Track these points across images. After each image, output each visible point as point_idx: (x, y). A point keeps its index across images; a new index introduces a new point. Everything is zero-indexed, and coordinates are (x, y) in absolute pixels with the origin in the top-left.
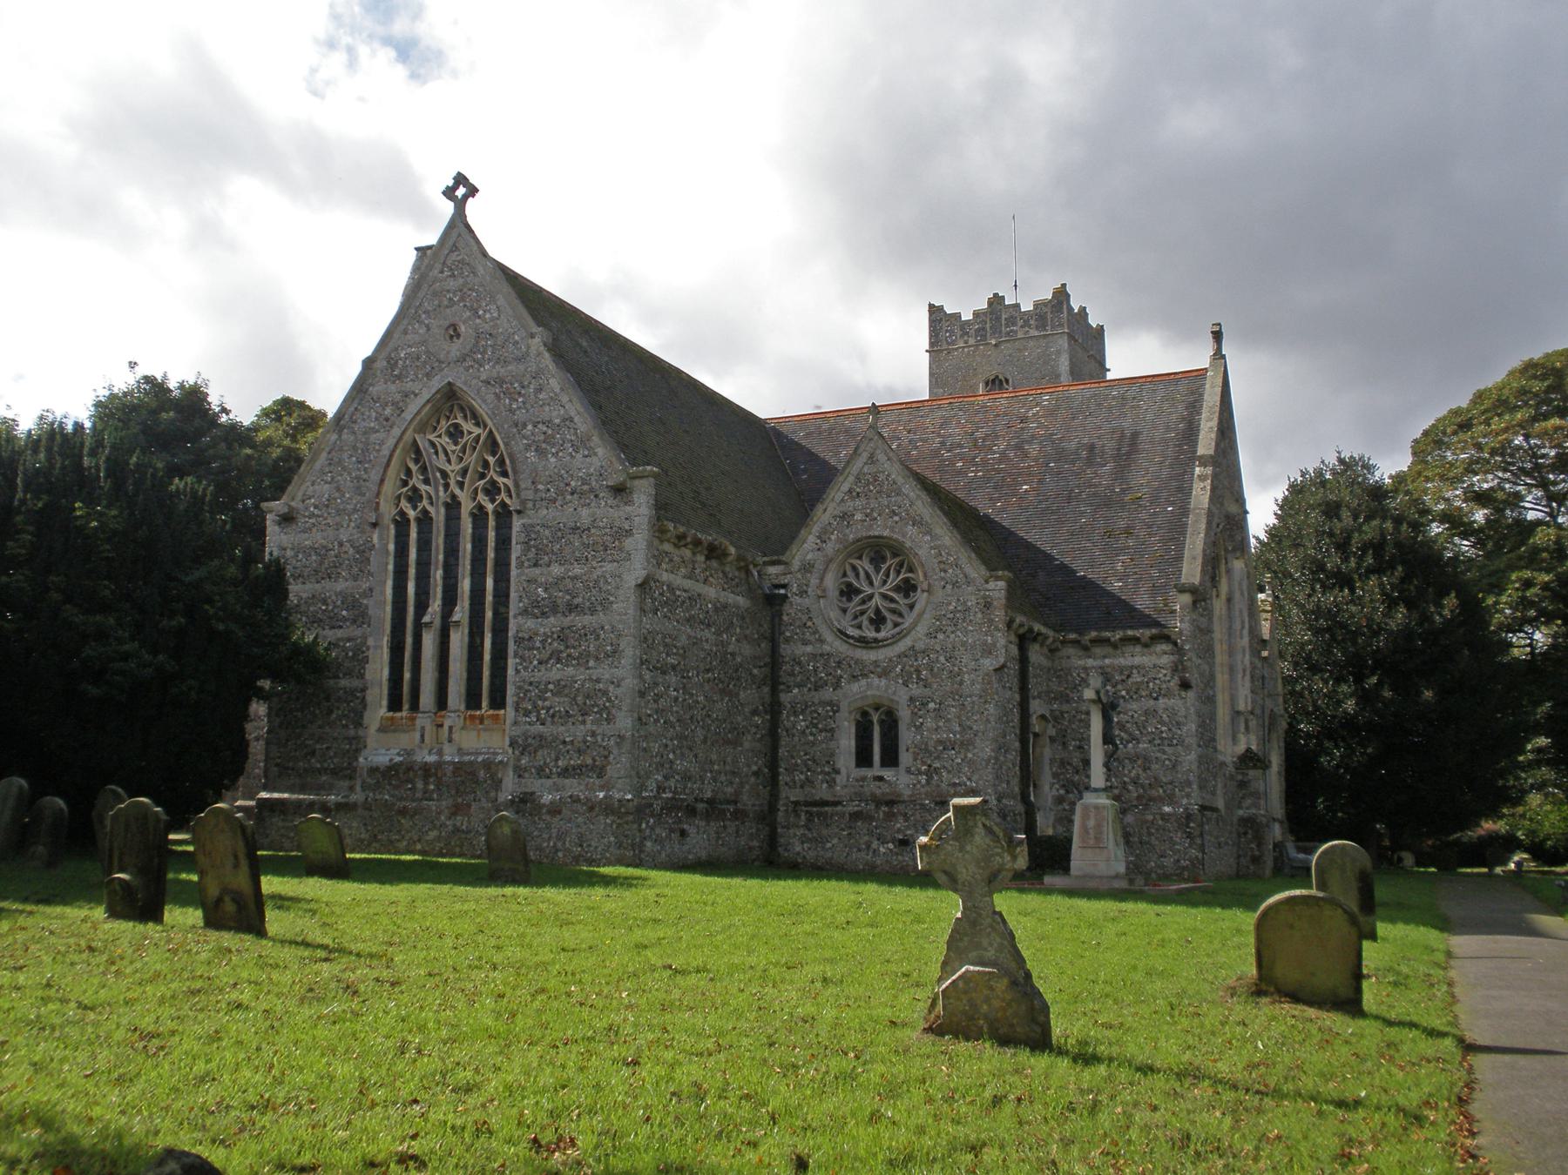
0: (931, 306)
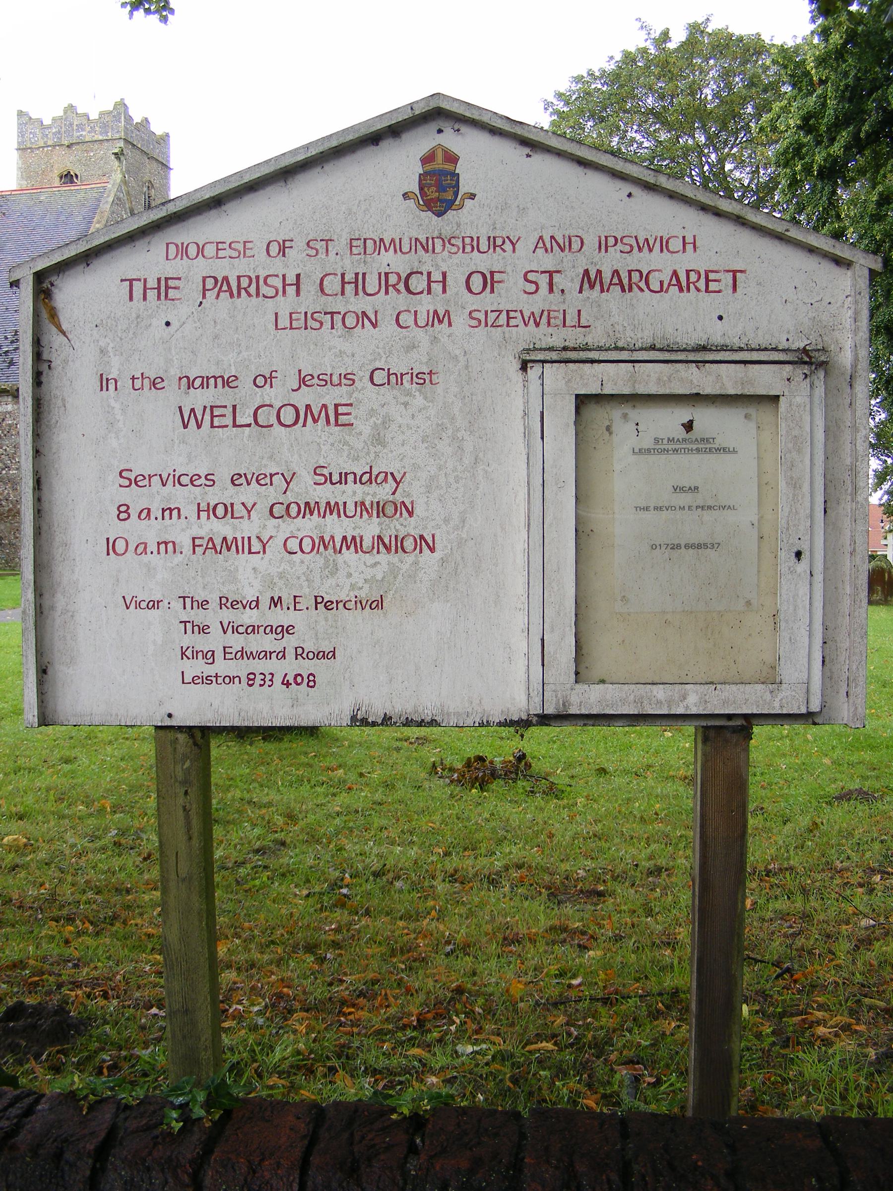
0: (20, 114)
